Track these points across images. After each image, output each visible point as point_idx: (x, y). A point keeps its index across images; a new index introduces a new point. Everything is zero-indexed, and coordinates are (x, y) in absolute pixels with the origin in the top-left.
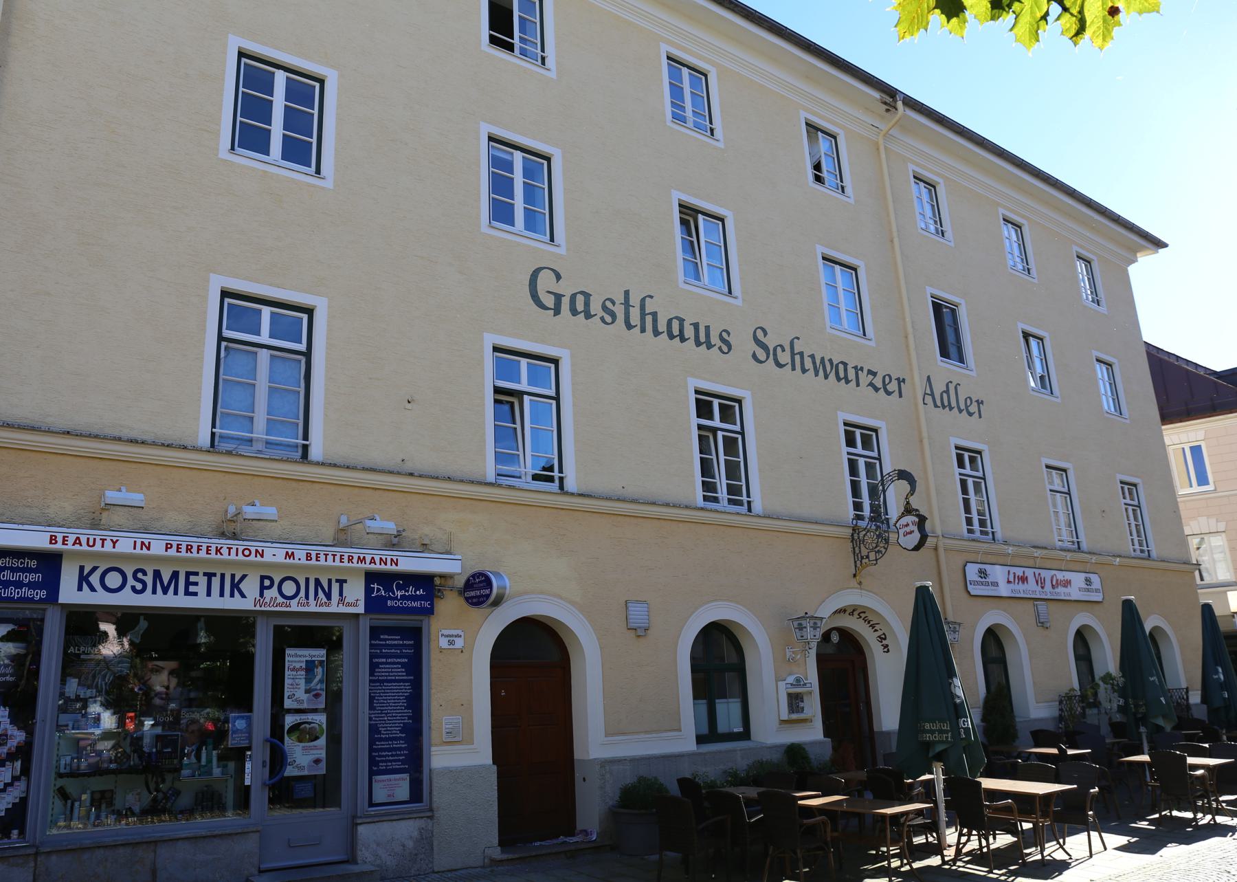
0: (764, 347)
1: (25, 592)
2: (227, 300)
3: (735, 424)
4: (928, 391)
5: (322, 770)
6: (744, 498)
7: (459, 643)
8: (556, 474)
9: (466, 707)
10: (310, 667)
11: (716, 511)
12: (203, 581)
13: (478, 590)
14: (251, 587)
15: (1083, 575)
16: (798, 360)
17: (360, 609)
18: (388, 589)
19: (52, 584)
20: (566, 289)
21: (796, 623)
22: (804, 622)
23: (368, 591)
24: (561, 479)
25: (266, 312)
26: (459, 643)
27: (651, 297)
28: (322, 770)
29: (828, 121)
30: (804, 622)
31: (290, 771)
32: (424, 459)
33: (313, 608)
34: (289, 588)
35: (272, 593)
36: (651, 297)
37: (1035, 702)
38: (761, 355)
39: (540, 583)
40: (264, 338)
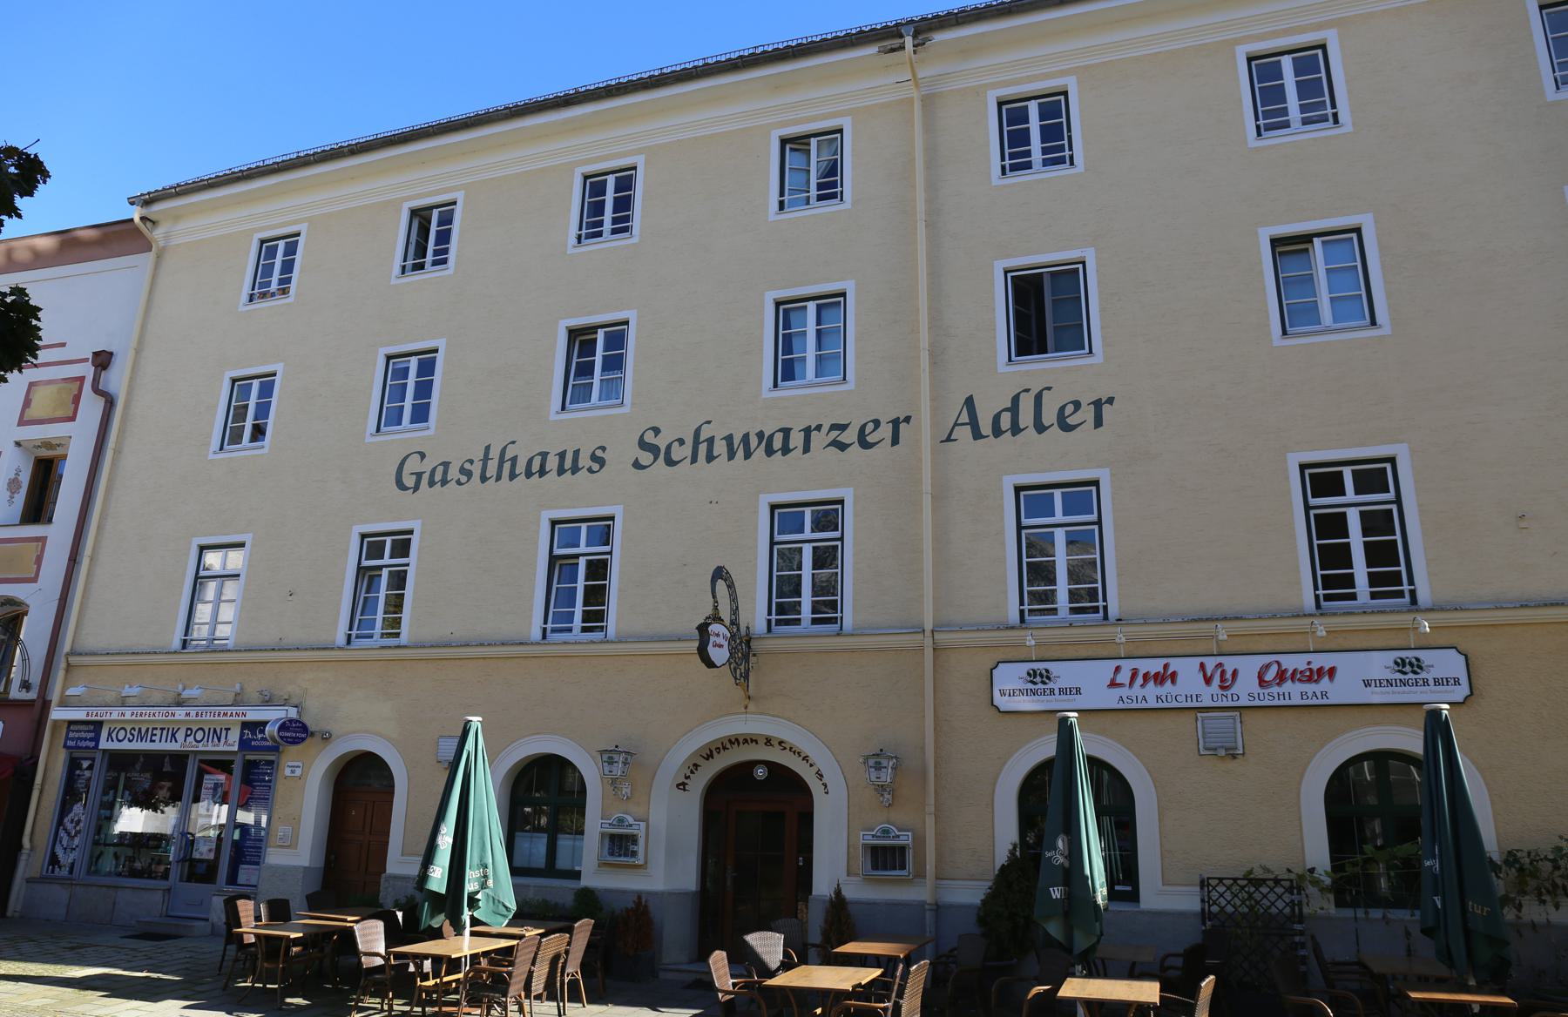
0: (654, 450)
1: (84, 744)
2: (1307, 472)
3: (392, 557)
4: (965, 418)
5: (212, 856)
6: (1406, 587)
7: (298, 772)
8: (1406, 587)
9: (296, 821)
10: (216, 786)
11: (398, 647)
12: (158, 732)
13: (296, 732)
14: (180, 736)
15: (1026, 667)
16: (702, 447)
17: (236, 748)
18: (254, 733)
19: (97, 739)
20: (427, 466)
21: (605, 757)
22: (616, 757)
23: (242, 734)
24: (1105, 608)
25: (1058, 493)
26: (298, 772)
27: (1049, 389)
28: (212, 856)
29: (1030, 79)
30: (616, 757)
31: (196, 855)
32: (295, 635)
33: (210, 748)
34: (199, 735)
35: (190, 739)
36: (1049, 389)
37: (1165, 893)
38: (646, 458)
39: (362, 720)
40: (1059, 517)
